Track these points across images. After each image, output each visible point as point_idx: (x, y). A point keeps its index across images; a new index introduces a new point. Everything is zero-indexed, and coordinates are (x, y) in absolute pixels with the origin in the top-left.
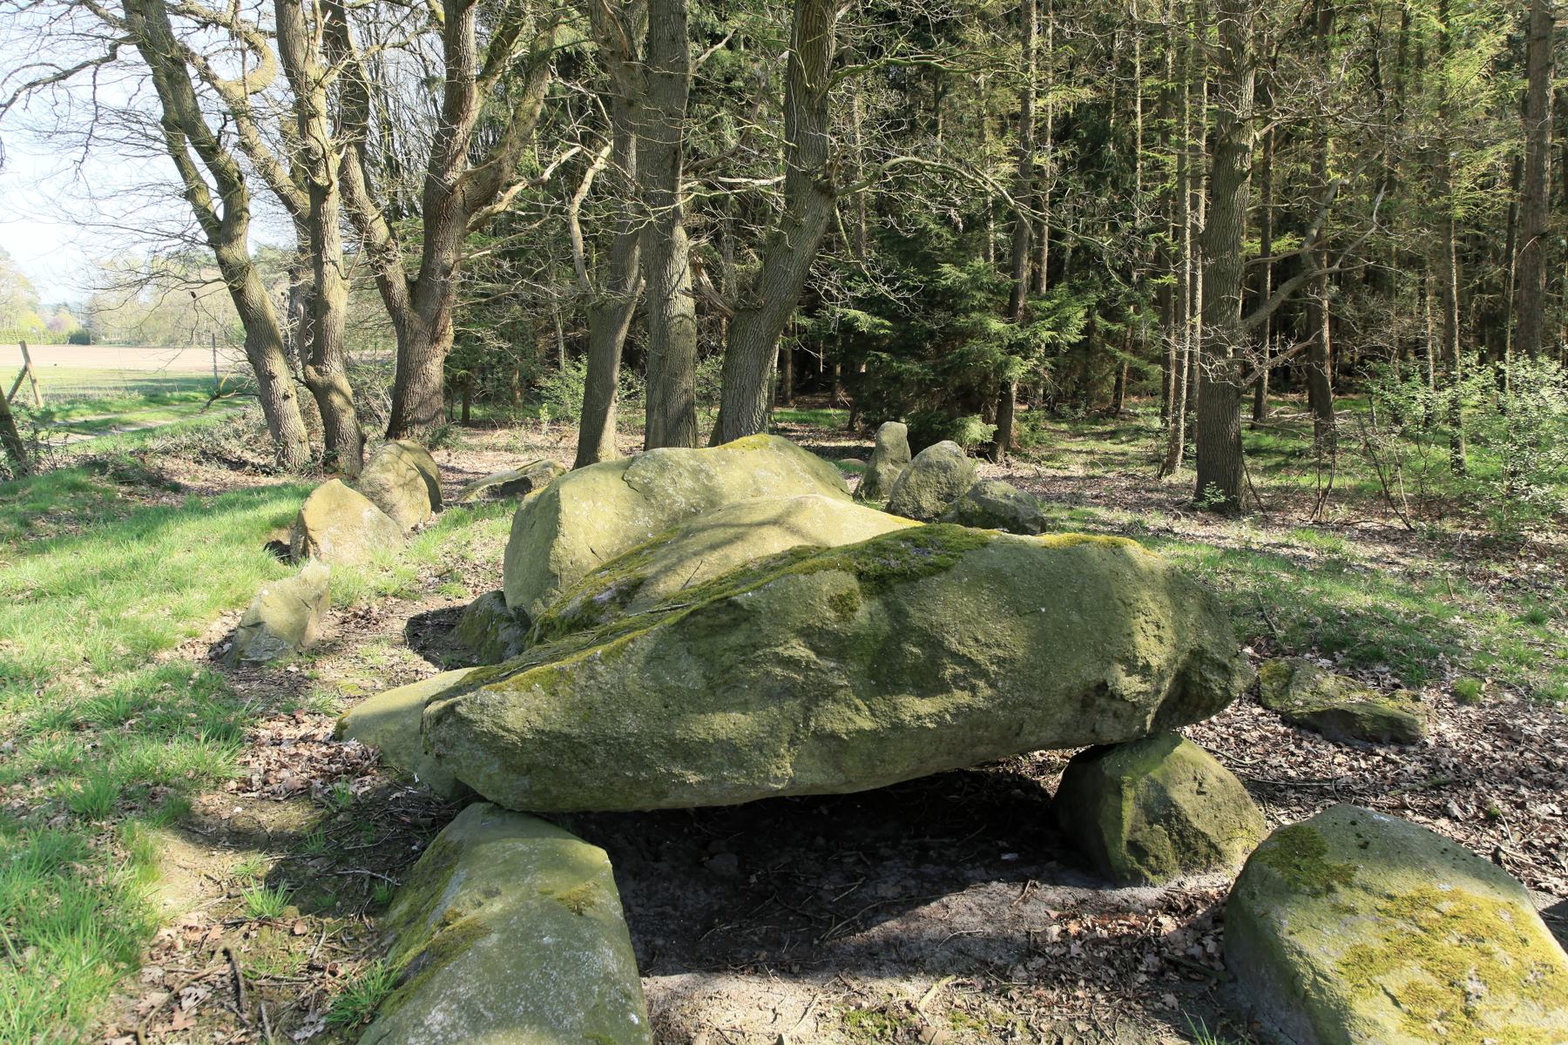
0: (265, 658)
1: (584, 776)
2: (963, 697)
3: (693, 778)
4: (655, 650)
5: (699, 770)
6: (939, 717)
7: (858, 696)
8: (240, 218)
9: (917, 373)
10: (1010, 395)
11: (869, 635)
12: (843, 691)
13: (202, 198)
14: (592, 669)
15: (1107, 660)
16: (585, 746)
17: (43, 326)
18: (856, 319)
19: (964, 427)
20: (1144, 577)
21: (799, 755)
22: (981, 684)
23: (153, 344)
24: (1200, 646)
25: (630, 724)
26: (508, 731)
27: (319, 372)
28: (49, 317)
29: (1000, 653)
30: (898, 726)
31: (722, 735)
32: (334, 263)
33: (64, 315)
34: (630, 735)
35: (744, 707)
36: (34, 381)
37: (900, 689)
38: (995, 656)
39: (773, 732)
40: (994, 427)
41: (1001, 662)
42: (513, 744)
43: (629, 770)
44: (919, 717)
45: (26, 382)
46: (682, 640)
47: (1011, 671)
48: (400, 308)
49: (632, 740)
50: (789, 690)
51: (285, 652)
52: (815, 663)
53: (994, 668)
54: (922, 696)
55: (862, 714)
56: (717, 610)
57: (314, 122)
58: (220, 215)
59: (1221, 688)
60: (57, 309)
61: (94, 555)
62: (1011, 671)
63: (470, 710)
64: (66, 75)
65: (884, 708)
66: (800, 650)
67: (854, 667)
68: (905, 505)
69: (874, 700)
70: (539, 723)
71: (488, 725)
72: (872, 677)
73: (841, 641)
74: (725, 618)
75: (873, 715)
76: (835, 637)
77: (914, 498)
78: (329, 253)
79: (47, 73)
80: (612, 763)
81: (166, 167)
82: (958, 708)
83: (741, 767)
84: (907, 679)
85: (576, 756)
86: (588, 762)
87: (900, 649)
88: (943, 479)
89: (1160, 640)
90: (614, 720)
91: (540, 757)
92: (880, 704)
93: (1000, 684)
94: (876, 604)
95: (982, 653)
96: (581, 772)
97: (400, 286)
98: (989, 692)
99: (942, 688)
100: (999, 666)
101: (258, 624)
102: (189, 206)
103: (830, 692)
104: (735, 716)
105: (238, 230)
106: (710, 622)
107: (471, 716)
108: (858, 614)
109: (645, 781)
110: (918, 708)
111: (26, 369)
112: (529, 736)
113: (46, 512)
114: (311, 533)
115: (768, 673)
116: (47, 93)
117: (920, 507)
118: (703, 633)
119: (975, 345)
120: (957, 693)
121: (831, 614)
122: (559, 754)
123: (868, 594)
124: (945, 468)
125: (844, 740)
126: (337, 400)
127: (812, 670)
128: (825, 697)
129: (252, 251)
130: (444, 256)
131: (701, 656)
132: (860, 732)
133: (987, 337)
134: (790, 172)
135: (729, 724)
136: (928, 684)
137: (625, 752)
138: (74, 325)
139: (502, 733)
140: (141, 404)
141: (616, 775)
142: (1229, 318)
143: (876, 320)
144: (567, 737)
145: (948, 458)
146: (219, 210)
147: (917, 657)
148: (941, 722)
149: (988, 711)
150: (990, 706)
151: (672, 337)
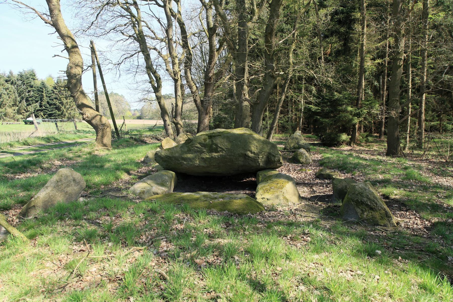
2: (221, 153)
3: (185, 163)
5: (186, 162)
6: (218, 156)
8: (160, 87)
9: (327, 122)
10: (356, 128)
13: (153, 83)
15: (247, 151)
17: (131, 115)
19: (340, 136)
20: (255, 139)
22: (224, 152)
25: (177, 155)
27: (176, 120)
28: (133, 112)
30: (212, 157)
31: (189, 157)
32: (179, 96)
33: (136, 112)
35: (192, 153)
36: (125, 125)
37: (213, 152)
39: (196, 157)
40: (350, 137)
41: (226, 148)
45: (124, 125)
48: (199, 106)
50: (198, 151)
51: (151, 162)
57: (175, 65)
58: (156, 86)
60: (135, 110)
61: (127, 149)
64: (133, 55)
66: (199, 146)
67: (207, 149)
70: (166, 154)
71: (160, 154)
76: (204, 144)
78: (178, 94)
79: (129, 55)
81: (147, 77)
89: (257, 149)
92: (210, 154)
94: (210, 140)
97: (199, 101)
101: (148, 157)
102: (150, 85)
103: (204, 152)
104: (191, 155)
105: (160, 89)
110: (215, 154)
111: (124, 122)
113: (121, 145)
116: (128, 60)
119: (343, 114)
121: (203, 141)
123: (209, 139)
124: (297, 139)
126: (179, 126)
129: (162, 94)
130: (209, 94)
132: (207, 157)
133: (347, 112)
134: (265, 73)
135: (190, 156)
136: (217, 152)
137: (176, 159)
138: (138, 114)
140: (148, 131)
142: (395, 104)
143: (317, 108)
145: (298, 136)
146: (156, 85)
148: (218, 157)
149: (225, 156)
151: (243, 110)
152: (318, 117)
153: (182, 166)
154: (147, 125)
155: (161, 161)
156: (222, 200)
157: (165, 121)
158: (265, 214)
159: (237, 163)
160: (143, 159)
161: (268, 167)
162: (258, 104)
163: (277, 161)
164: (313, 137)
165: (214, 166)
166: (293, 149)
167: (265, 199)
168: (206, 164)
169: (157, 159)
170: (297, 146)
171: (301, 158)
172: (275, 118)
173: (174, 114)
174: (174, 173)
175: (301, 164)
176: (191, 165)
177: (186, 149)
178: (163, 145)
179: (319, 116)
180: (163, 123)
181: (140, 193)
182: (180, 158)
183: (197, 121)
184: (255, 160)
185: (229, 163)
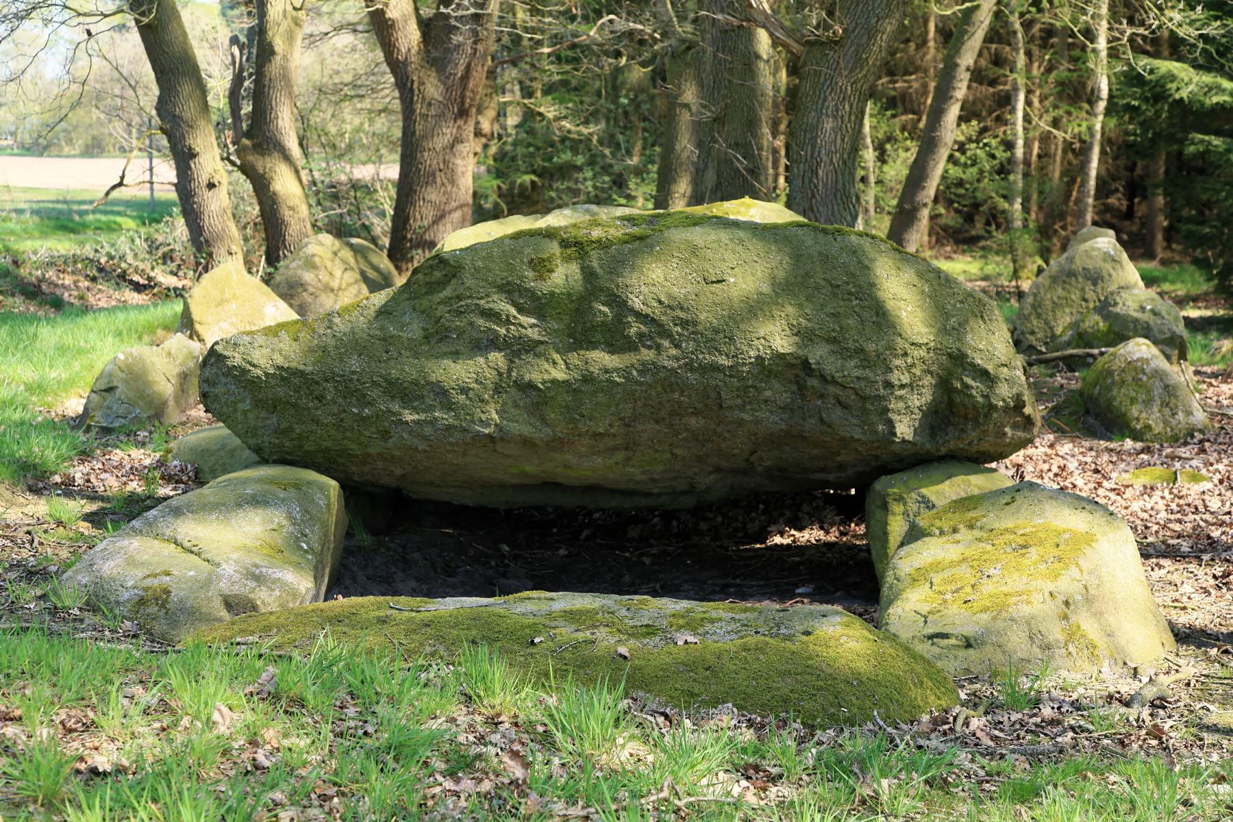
0: (116, 425)
1: (319, 412)
2: (647, 355)
3: (409, 417)
4: (385, 305)
5: (415, 410)
7: (558, 352)
11: (562, 294)
12: (542, 347)
14: (330, 321)
16: (317, 383)
18: (1172, 77)
21: (504, 404)
22: (666, 343)
23: (67, 150)
24: (959, 350)
26: (254, 366)
29: (682, 315)
30: (587, 379)
34: (354, 373)
37: (593, 346)
38: (678, 317)
42: (258, 377)
43: (355, 406)
44: (607, 371)
46: (408, 299)
47: (693, 333)
49: (355, 377)
52: (515, 317)
53: (679, 329)
54: (612, 353)
55: (558, 367)
56: (431, 267)
59: (983, 396)
62: (693, 333)
63: (225, 348)
65: (577, 362)
68: (1033, 333)
69: (570, 355)
70: (279, 360)
72: (569, 336)
73: (539, 298)
74: (438, 274)
75: (568, 368)
77: (1047, 323)
80: (341, 400)
82: (643, 364)
83: (450, 409)
84: (598, 336)
85: (311, 393)
86: (320, 398)
87: (591, 308)
88: (1090, 295)
90: (342, 360)
91: (281, 392)
92: (574, 358)
93: (684, 345)
95: (665, 314)
96: (316, 409)
98: (674, 352)
99: (629, 346)
100: (683, 328)
106: (428, 279)
107: (226, 353)
108: (554, 275)
109: (368, 417)
110: (601, 359)
112: (272, 371)
114: (197, 327)
115: (471, 324)
117: (1054, 337)
118: (424, 291)
120: (644, 351)
122: (297, 390)
124: (1095, 278)
125: (540, 390)
127: (513, 324)
128: (527, 352)
131: (423, 312)
137: (351, 389)
139: (249, 367)
141: (345, 411)
144: (302, 373)
147: (605, 315)
150: (676, 365)
152: (1216, 141)
153: (385, 435)
154: (25, 190)
155: (246, 405)
156: (691, 639)
157: (184, 158)
158: (966, 723)
159: (745, 416)
160: (74, 405)
161: (943, 450)
162: (835, 43)
163: (1006, 409)
164: (1165, 279)
165: (597, 436)
166: (1069, 344)
167: (953, 641)
168: (543, 420)
169: (219, 390)
170: (1095, 322)
171: (1133, 401)
172: (928, 145)
173: (247, 108)
174: (333, 484)
175: (1136, 437)
176: (449, 428)
177: (414, 329)
178: (196, 314)
179: (1217, 133)
180: (166, 172)
181: (142, 602)
182: (376, 384)
183: (392, 171)
184: (864, 399)
185: (693, 421)
